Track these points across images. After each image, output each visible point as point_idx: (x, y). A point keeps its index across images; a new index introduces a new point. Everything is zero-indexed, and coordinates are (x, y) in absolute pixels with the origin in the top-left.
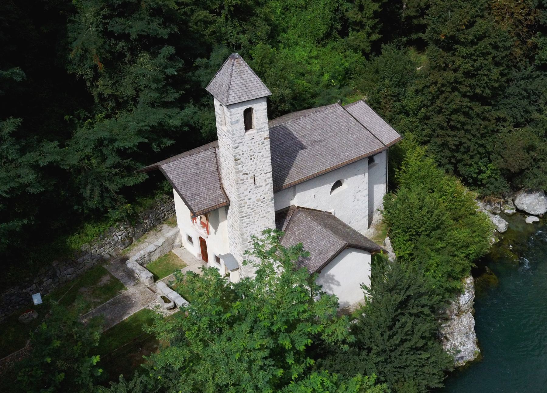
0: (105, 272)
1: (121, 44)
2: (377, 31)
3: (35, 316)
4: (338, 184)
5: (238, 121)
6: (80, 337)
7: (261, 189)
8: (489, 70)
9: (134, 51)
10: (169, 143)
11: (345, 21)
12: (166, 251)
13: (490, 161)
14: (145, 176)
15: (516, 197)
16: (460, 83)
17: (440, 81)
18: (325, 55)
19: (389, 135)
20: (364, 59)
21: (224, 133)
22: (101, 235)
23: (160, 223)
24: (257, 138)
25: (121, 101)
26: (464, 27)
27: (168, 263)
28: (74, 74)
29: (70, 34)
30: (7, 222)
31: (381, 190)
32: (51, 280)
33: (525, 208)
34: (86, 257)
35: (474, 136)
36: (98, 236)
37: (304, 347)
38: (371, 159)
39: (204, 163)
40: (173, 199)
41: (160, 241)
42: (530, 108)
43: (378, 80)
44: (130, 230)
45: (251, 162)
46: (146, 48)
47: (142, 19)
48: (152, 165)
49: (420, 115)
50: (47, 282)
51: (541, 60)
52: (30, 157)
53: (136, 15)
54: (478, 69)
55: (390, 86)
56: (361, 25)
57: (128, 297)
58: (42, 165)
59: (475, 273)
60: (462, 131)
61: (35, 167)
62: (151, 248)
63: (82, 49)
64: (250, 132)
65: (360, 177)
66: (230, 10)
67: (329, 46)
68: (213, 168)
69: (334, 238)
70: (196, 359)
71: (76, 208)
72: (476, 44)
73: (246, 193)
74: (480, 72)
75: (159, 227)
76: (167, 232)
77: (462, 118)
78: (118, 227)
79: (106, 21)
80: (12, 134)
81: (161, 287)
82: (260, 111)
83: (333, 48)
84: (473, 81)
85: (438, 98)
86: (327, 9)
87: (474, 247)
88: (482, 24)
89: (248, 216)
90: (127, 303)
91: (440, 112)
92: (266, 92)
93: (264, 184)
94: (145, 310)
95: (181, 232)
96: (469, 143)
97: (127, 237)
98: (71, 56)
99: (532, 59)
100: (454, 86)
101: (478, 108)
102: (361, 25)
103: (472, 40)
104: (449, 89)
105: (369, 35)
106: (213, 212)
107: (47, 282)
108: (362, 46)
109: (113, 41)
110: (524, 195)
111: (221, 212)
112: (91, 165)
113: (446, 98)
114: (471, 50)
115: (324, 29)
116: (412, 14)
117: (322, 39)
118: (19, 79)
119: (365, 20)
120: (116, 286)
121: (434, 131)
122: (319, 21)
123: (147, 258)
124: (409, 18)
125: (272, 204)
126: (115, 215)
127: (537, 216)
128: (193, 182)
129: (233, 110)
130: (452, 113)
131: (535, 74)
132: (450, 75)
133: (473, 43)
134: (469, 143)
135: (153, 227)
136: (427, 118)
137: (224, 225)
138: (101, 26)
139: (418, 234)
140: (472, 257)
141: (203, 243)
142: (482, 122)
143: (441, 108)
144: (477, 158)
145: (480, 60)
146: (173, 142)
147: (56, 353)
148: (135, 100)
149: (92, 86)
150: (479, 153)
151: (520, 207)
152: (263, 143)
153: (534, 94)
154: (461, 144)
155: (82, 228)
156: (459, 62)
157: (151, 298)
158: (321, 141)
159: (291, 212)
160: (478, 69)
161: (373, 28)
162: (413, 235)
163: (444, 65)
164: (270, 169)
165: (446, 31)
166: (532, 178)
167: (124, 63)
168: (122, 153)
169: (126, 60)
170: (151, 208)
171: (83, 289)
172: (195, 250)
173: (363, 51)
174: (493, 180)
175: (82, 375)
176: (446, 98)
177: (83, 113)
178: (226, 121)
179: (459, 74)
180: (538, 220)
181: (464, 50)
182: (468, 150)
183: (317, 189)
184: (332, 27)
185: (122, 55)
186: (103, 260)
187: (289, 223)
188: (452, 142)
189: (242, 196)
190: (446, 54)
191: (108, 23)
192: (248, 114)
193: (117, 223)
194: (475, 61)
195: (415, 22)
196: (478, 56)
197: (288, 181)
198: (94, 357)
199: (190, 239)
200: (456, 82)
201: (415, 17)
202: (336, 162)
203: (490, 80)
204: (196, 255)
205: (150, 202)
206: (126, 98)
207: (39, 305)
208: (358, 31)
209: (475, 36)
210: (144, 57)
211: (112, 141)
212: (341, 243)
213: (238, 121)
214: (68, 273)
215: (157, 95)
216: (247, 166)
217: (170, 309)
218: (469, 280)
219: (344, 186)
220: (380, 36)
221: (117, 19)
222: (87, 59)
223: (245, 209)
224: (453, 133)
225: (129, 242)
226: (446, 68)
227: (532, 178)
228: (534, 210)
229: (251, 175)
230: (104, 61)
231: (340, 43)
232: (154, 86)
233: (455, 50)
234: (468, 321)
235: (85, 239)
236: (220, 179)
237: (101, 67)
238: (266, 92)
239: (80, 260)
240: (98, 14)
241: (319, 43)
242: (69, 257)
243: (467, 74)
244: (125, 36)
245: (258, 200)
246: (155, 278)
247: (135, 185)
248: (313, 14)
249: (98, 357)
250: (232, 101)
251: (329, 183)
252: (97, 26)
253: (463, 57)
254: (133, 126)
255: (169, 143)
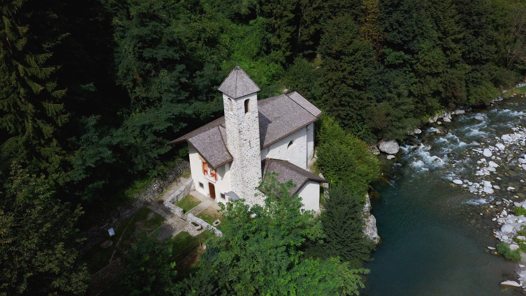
0: (149, 211)
1: (149, 65)
2: (289, 50)
3: (111, 243)
4: (291, 143)
5: (241, 108)
6: (161, 251)
7: (253, 149)
8: (362, 70)
9: (157, 69)
10: (184, 125)
11: (268, 45)
12: (186, 194)
13: (364, 124)
14: (170, 147)
15: (379, 145)
16: (347, 78)
17: (334, 78)
18: (258, 66)
19: (316, 112)
20: (282, 67)
21: (230, 116)
22: (145, 187)
23: (178, 177)
24: (252, 118)
25: (151, 100)
26: (346, 45)
27: (189, 202)
28: (120, 86)
29: (116, 60)
30: (93, 183)
31: (311, 144)
32: (117, 219)
33: (385, 150)
34: (137, 202)
35: (355, 109)
36: (143, 188)
37: (300, 244)
38: (307, 126)
39: (214, 136)
40: (189, 161)
41: (183, 188)
42: (386, 90)
43: (296, 80)
44: (162, 182)
45: (248, 133)
46: (164, 67)
47: (163, 48)
48: (173, 141)
49: (323, 99)
50: (115, 220)
51: (389, 62)
52: (106, 139)
53: (160, 46)
54: (356, 69)
55: (304, 82)
56: (279, 47)
57: (169, 226)
58: (114, 144)
59: (369, 191)
60: (348, 107)
61: (110, 147)
62: (178, 192)
63: (126, 69)
64: (247, 114)
65: (302, 137)
66: (205, 41)
67: (260, 61)
68: (220, 139)
69: (298, 176)
70: (237, 258)
71: (129, 171)
72: (354, 55)
73: (245, 152)
74: (357, 71)
75: (178, 179)
76: (184, 183)
77: (348, 99)
78: (155, 181)
79: (141, 51)
80: (95, 126)
81: (190, 217)
82: (253, 100)
83: (262, 62)
84: (353, 77)
85: (333, 88)
86: (258, 38)
87: (371, 175)
88: (357, 43)
89: (246, 167)
90: (169, 229)
91: (334, 96)
92: (257, 89)
93: (255, 146)
94: (182, 232)
95: (194, 181)
96: (352, 114)
97: (160, 187)
98: (119, 73)
99: (383, 62)
100: (343, 80)
101: (357, 93)
102: (279, 47)
103: (352, 52)
104: (339, 83)
105: (284, 52)
106: (220, 166)
107: (115, 220)
108: (281, 59)
109: (144, 63)
110: (384, 142)
111: (227, 166)
112: (136, 142)
113: (338, 88)
114: (352, 58)
115: (256, 50)
116: (305, 39)
117: (255, 56)
118: (93, 90)
119: (281, 44)
120: (159, 220)
121: (331, 108)
122: (253, 46)
123: (175, 200)
124: (303, 41)
125: (260, 158)
126: (155, 173)
127: (393, 154)
128: (209, 148)
129: (239, 101)
130: (342, 97)
131: (385, 71)
132: (341, 75)
133: (352, 54)
134: (352, 114)
135: (174, 180)
136: (327, 100)
137: (228, 174)
138: (137, 54)
139: (340, 170)
140: (370, 181)
141: (212, 187)
142: (359, 101)
143: (335, 94)
144: (356, 123)
145: (357, 64)
146: (187, 124)
147: (146, 264)
148: (160, 99)
149: (131, 92)
150: (358, 119)
151: (383, 150)
152: (255, 121)
153: (386, 82)
154: (348, 114)
155: (133, 184)
156: (345, 66)
157: (185, 224)
158: (279, 117)
159: (267, 162)
160: (356, 69)
161: (287, 48)
162: (337, 171)
163: (335, 68)
164: (258, 136)
165: (336, 48)
166: (389, 132)
167: (151, 77)
168: (156, 133)
169: (152, 74)
170: (173, 168)
171: (138, 223)
172: (205, 192)
173: (281, 62)
174: (367, 135)
175: (165, 277)
176: (338, 88)
177: (126, 110)
178: (232, 109)
179: (346, 73)
180: (394, 157)
181: (347, 59)
182: (352, 118)
183: (281, 147)
184: (261, 49)
185: (149, 72)
186: (147, 203)
187: (267, 169)
188: (343, 114)
189: (243, 154)
190: (336, 62)
191: (142, 52)
192: (246, 102)
193: (154, 179)
194: (354, 65)
195: (307, 43)
196: (356, 62)
197: (266, 143)
198: (171, 263)
199: (201, 185)
200: (344, 78)
201: (307, 41)
202: (291, 130)
203: (363, 75)
204: (206, 195)
205: (172, 164)
206: (154, 99)
207: (113, 236)
208: (277, 50)
209: (353, 50)
210: (164, 73)
211: (151, 126)
212: (305, 178)
213: (241, 108)
214: (127, 214)
215: (175, 96)
216: (246, 135)
217: (199, 230)
218: (367, 196)
219: (294, 144)
220: (291, 53)
221: (147, 49)
222: (129, 75)
223: (245, 162)
224: (343, 109)
225: (161, 190)
226: (337, 70)
227: (389, 132)
228: (391, 151)
229: (248, 140)
230: (141, 76)
231: (266, 58)
232: (173, 90)
233: (342, 59)
234: (372, 220)
235: (136, 190)
236: (225, 145)
237: (140, 80)
238: (257, 89)
239: (134, 204)
240: (135, 46)
241: (253, 59)
242: (127, 203)
243: (350, 73)
244: (153, 60)
245: (252, 156)
246: (184, 212)
247: (165, 154)
248: (249, 42)
249: (174, 263)
250: (238, 95)
251: (287, 143)
252: (135, 54)
253: (347, 63)
254: (165, 116)
255: (184, 125)
